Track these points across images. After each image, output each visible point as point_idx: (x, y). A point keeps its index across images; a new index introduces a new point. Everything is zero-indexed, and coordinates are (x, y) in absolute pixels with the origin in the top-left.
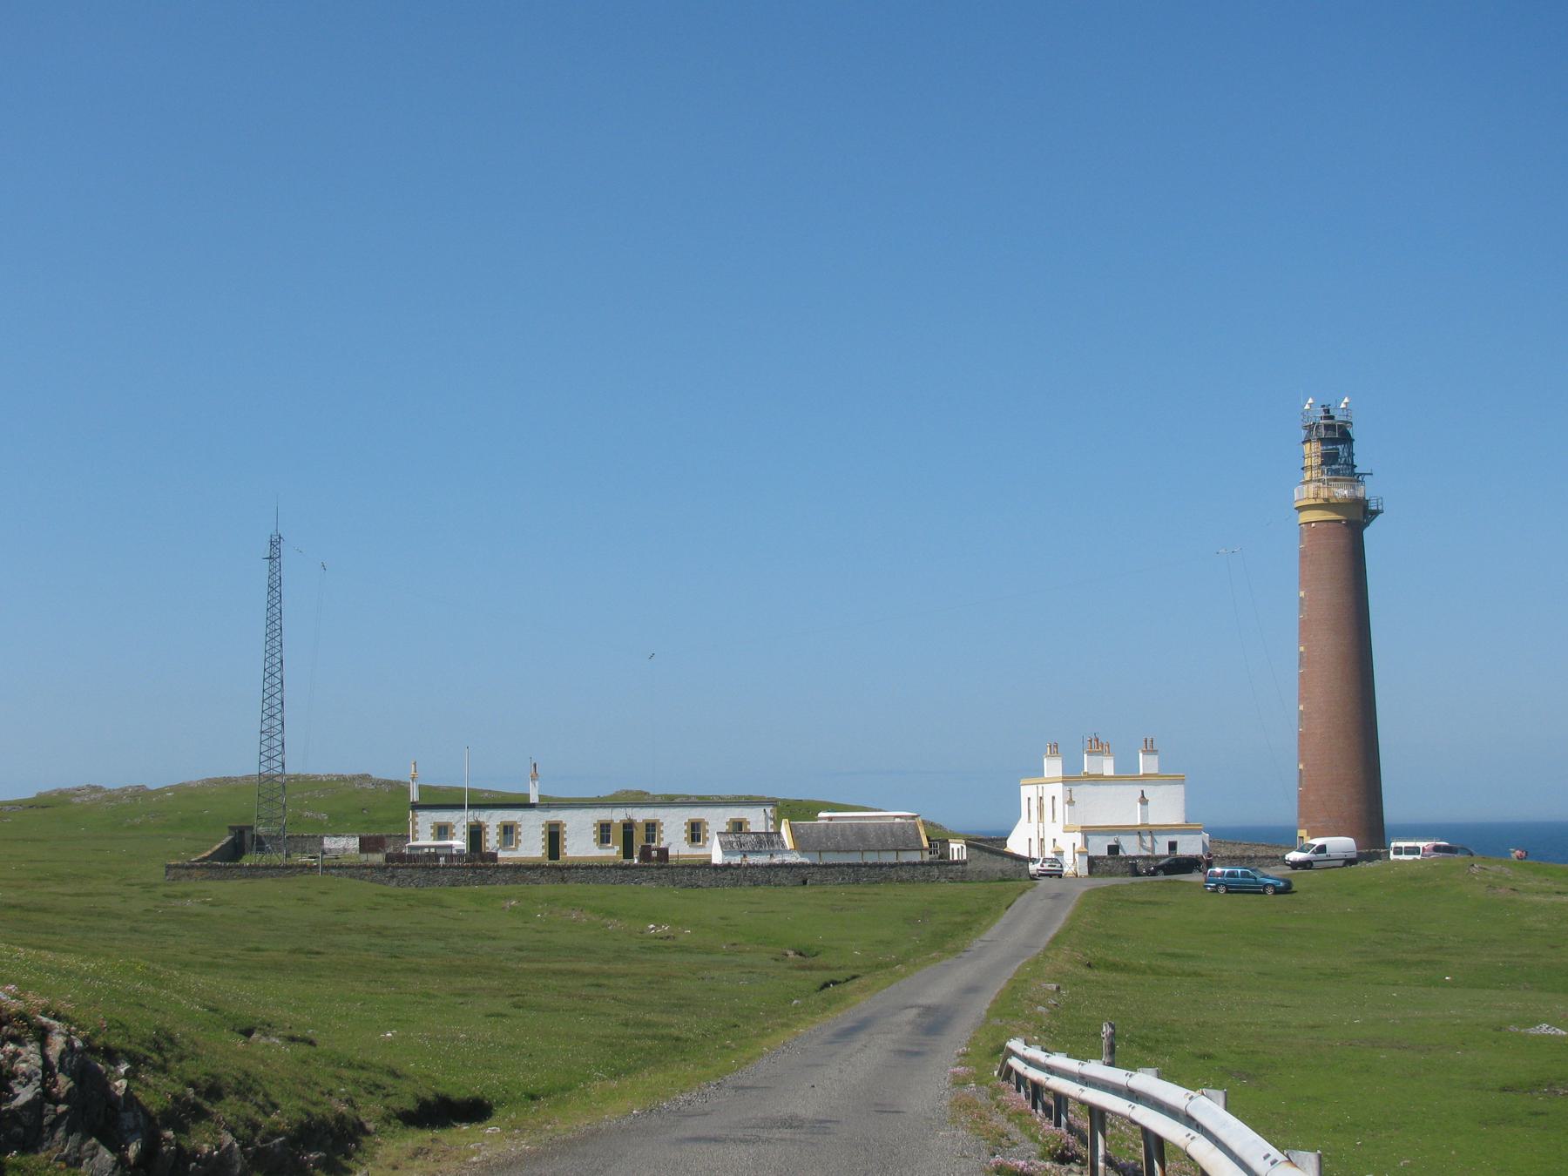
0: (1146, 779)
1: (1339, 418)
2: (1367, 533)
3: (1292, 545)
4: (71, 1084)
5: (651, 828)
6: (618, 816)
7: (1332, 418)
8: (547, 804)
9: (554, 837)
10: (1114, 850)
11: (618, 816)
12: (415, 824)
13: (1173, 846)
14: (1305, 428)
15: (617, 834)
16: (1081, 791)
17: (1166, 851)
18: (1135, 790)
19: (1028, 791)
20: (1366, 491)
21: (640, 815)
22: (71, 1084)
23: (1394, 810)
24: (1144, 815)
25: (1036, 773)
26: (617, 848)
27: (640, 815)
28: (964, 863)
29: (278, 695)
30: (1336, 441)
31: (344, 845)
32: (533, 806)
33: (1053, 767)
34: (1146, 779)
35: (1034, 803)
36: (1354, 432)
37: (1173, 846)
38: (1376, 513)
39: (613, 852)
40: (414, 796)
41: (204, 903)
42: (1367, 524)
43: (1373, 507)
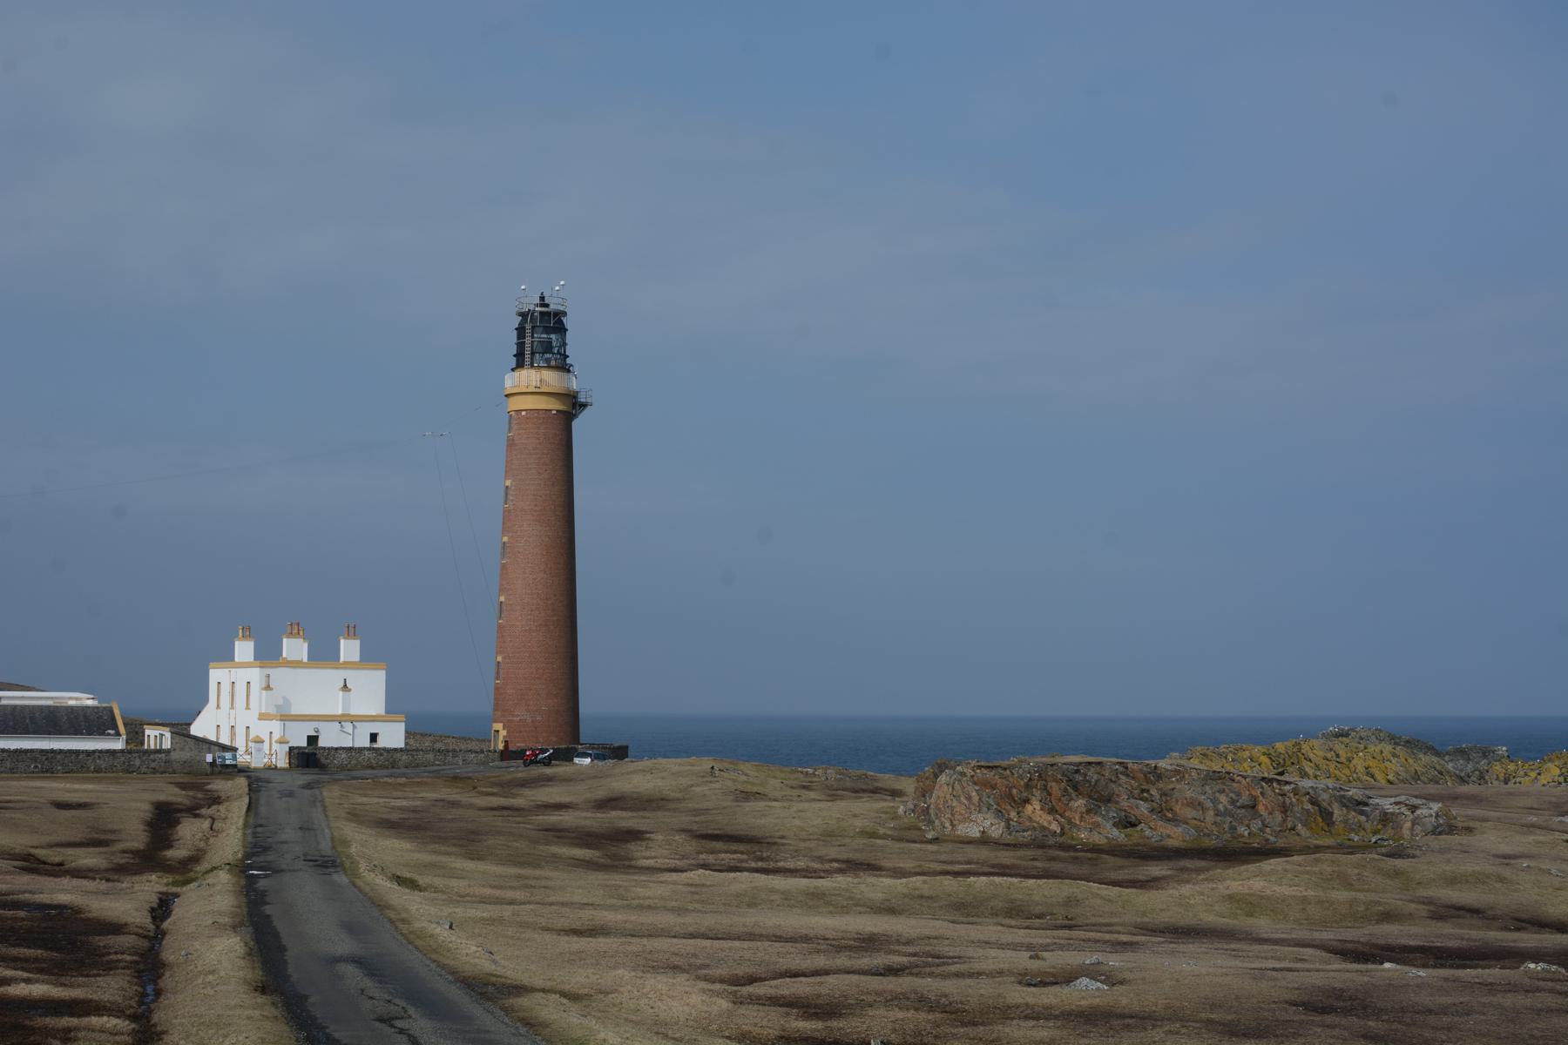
0: (348, 665)
2: (575, 424)
10: (313, 740)
13: (374, 737)
16: (277, 673)
19: (217, 675)
24: (346, 703)
25: (226, 657)
28: (168, 751)
29: (251, 821)
30: (542, 334)
33: (244, 649)
35: (226, 688)
37: (374, 737)
38: (584, 406)
42: (575, 416)
43: (582, 399)
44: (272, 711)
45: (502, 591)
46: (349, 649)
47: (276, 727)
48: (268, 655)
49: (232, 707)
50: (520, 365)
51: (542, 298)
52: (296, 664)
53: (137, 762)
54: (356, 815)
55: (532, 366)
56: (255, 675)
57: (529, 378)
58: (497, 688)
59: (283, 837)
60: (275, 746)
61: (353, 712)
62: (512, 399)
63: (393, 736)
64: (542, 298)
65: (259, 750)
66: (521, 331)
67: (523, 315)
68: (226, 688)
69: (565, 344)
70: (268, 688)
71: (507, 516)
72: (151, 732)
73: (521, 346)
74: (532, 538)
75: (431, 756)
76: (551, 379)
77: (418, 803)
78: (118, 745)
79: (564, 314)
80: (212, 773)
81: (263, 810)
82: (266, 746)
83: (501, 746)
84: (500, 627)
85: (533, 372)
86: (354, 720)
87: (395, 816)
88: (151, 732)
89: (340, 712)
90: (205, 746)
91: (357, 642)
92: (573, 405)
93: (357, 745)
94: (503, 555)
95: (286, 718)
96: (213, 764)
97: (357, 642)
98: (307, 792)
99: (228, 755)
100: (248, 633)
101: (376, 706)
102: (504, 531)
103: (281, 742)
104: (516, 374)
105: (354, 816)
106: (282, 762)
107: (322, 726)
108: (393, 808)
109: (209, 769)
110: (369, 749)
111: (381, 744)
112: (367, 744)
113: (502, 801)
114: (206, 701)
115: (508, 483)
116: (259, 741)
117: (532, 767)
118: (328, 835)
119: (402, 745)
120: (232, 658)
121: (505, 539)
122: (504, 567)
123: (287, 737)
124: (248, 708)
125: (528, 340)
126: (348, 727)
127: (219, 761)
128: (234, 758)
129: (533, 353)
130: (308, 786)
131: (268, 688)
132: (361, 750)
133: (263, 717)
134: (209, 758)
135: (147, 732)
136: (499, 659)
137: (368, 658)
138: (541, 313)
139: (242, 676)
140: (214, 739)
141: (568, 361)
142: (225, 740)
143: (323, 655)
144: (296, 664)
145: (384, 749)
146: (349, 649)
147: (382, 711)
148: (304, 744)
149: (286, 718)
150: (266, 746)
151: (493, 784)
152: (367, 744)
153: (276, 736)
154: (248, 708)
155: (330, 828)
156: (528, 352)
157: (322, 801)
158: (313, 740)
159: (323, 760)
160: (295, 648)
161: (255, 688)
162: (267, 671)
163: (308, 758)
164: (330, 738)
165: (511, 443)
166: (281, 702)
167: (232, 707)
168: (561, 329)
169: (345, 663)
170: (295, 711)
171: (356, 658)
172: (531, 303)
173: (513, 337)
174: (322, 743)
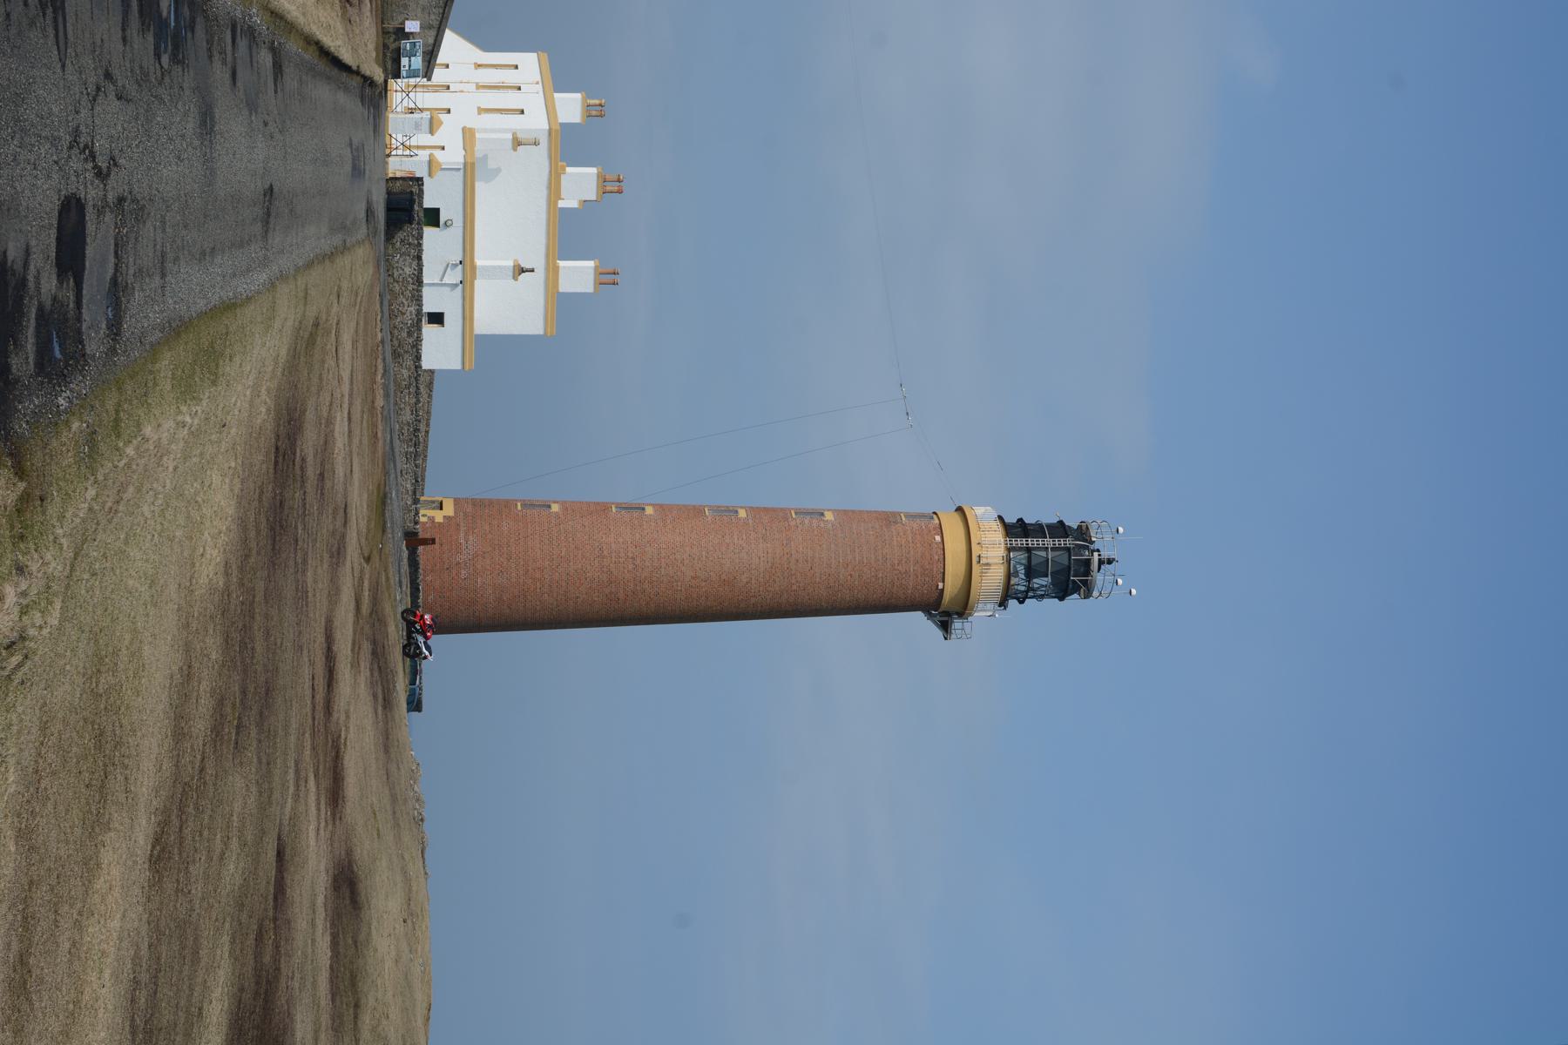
0: (552, 273)
1: (1100, 578)
2: (919, 616)
3: (905, 493)
10: (433, 217)
13: (437, 318)
16: (537, 160)
17: (429, 307)
18: (536, 259)
19: (529, 64)
20: (982, 613)
24: (494, 272)
25: (559, 79)
29: (293, 46)
30: (1057, 563)
33: (570, 106)
34: (552, 273)
35: (509, 77)
36: (1073, 600)
37: (437, 318)
38: (945, 627)
41: (349, 703)
42: (930, 616)
43: (957, 624)
44: (479, 150)
45: (660, 508)
46: (578, 275)
47: (453, 156)
48: (567, 145)
49: (479, 87)
50: (1017, 529)
51: (1110, 561)
52: (554, 190)
54: (311, 341)
55: (1009, 550)
56: (535, 121)
57: (993, 546)
58: (508, 504)
59: (232, 123)
60: (423, 155)
61: (479, 284)
62: (957, 517)
63: (440, 350)
64: (1110, 561)
65: (417, 126)
66: (1060, 529)
67: (1082, 533)
68: (509, 77)
70: (517, 143)
71: (777, 515)
73: (1038, 530)
74: (749, 559)
75: (407, 416)
76: (991, 578)
77: (340, 471)
79: (1088, 595)
80: (385, 32)
81: (323, 93)
82: (423, 139)
84: (604, 508)
85: (1001, 552)
87: (309, 441)
89: (479, 262)
90: (434, 20)
91: (590, 288)
92: (947, 613)
93: (426, 291)
94: (718, 510)
95: (469, 172)
96: (401, 33)
97: (590, 288)
98: (361, 209)
99: (418, 62)
100: (594, 113)
101: (485, 323)
102: (754, 511)
103: (431, 163)
104: (997, 527)
105: (309, 341)
106: (397, 166)
107: (456, 232)
108: (330, 422)
109: (392, 25)
110: (419, 312)
111: (428, 330)
112: (427, 308)
113: (343, 647)
114: (486, 47)
115: (829, 516)
116: (432, 127)
117: (402, 625)
118: (243, 286)
119: (426, 364)
120: (560, 86)
121: (742, 514)
122: (698, 511)
123: (439, 175)
124: (481, 111)
125: (1049, 542)
126: (454, 277)
127: (406, 45)
128: (413, 74)
129: (1028, 550)
130: (370, 212)
131: (517, 143)
132: (418, 299)
133: (468, 135)
134: (412, 26)
136: (555, 508)
137: (561, 305)
138: (1088, 562)
139: (532, 98)
141: (1013, 603)
143: (568, 231)
144: (554, 190)
145: (419, 339)
146: (578, 275)
148: (428, 204)
149: (469, 172)
150: (423, 139)
151: (375, 601)
152: (427, 308)
153: (438, 154)
154: (481, 111)
155: (272, 286)
156: (1032, 542)
157: (344, 249)
158: (433, 217)
159: (400, 235)
160: (581, 183)
161: (514, 122)
163: (405, 210)
164: (437, 246)
165: (889, 519)
166: (492, 164)
167: (479, 87)
169: (556, 269)
170: (480, 187)
171: (565, 286)
172: (1103, 543)
173: (1049, 518)
174: (429, 232)
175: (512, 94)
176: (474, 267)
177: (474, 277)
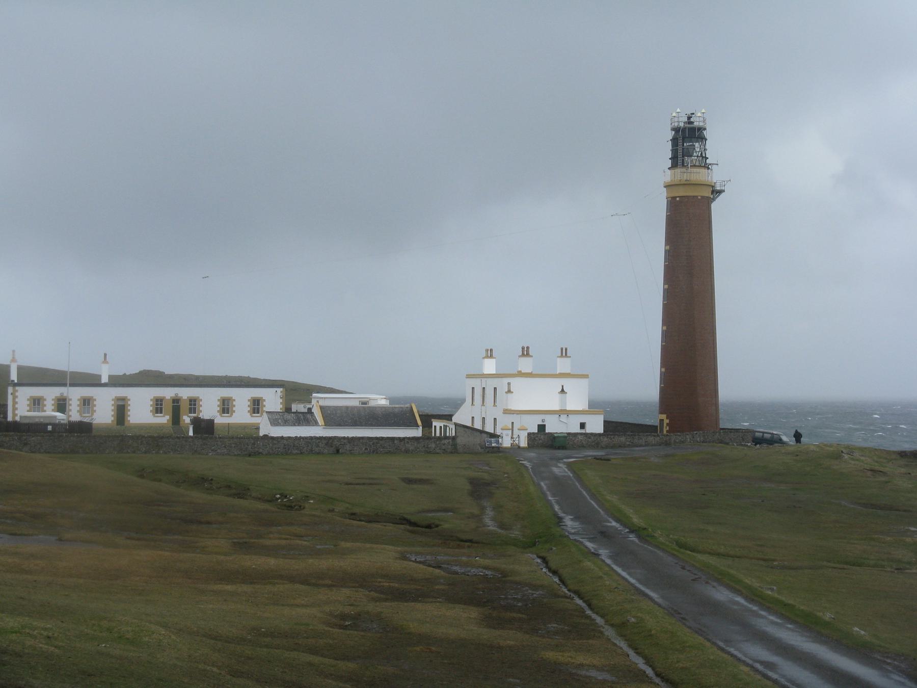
2: (714, 206)
4: (10, 419)
5: (193, 403)
6: (168, 393)
7: (692, 123)
8: (117, 381)
9: (121, 410)
10: (542, 428)
11: (168, 393)
12: (15, 397)
13: (583, 426)
14: (673, 129)
15: (168, 407)
18: (557, 384)
21: (185, 393)
22: (10, 419)
23: (557, 408)
24: (563, 402)
26: (168, 417)
27: (185, 393)
28: (454, 438)
31: (278, 496)
32: (105, 385)
35: (478, 392)
37: (583, 426)
39: (164, 419)
40: (14, 377)
42: (714, 199)
51: (689, 118)
53: (433, 446)
63: (596, 425)
66: (675, 141)
68: (478, 392)
69: (705, 150)
70: (509, 391)
72: (437, 424)
78: (417, 432)
83: (438, 434)
86: (568, 413)
88: (437, 424)
106: (524, 443)
111: (589, 429)
132: (576, 434)
135: (434, 424)
140: (469, 424)
142: (489, 428)
145: (592, 434)
147: (586, 408)
158: (542, 428)
162: (583, 431)
164: (554, 427)
168: (702, 139)
172: (682, 122)
175: (487, 392)
176: (561, 410)
177: (566, 410)
